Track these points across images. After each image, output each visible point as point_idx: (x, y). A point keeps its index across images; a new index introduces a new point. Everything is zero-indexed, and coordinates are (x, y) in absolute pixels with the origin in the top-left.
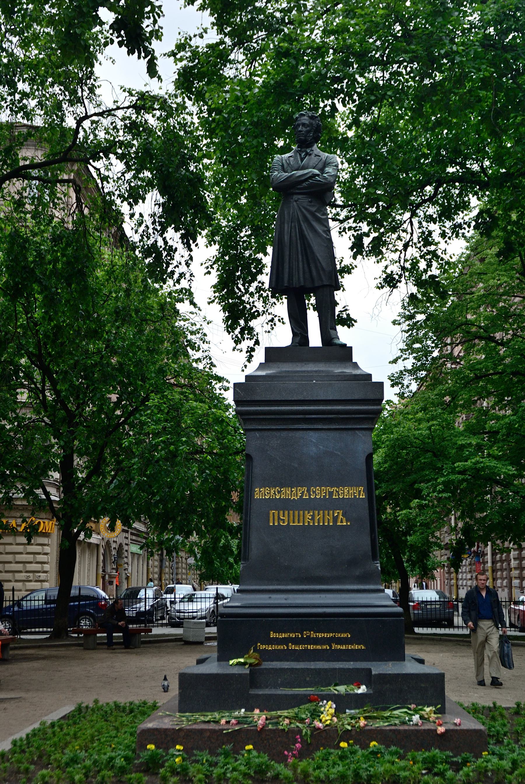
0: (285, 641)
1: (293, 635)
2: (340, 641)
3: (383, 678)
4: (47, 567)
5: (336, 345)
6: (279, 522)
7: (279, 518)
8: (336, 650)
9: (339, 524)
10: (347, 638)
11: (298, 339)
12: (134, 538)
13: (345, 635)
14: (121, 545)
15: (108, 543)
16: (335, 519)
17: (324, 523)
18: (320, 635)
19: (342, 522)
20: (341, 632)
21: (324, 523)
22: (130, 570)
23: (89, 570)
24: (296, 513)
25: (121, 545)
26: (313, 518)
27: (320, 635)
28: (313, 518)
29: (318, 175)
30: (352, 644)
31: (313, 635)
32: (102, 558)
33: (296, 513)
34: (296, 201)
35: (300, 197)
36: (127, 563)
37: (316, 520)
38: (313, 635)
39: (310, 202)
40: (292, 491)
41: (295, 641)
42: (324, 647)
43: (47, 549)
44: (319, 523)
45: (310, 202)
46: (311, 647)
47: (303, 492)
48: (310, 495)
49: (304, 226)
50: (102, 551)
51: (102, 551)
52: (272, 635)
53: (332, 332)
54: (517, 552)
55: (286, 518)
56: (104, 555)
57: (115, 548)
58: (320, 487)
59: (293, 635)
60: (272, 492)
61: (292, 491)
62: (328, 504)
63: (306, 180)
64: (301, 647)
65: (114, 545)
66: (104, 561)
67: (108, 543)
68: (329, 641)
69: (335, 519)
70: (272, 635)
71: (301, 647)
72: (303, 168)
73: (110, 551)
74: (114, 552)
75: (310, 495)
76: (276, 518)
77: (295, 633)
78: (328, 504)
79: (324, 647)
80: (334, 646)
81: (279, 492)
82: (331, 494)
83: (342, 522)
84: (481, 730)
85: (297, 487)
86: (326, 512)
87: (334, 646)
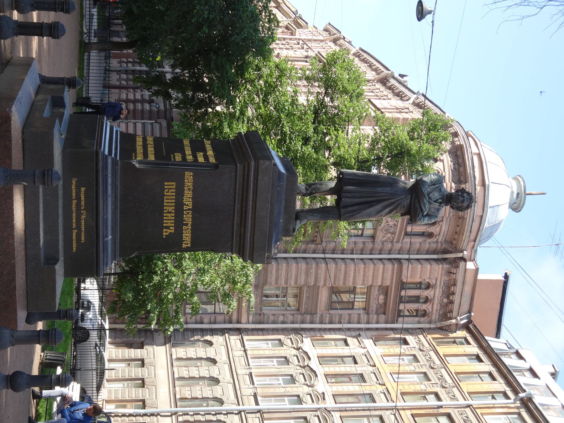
0: (78, 198)
9: (164, 230)
10: (81, 240)
16: (168, 228)
18: (83, 222)
19: (166, 232)
26: (169, 212)
27: (83, 222)
31: (83, 217)
33: (174, 201)
35: (409, 201)
38: (83, 217)
40: (189, 198)
41: (78, 205)
42: (74, 225)
44: (166, 216)
52: (83, 189)
60: (189, 184)
61: (189, 198)
63: (420, 206)
69: (168, 228)
70: (83, 189)
75: (186, 210)
77: (85, 205)
78: (179, 223)
79: (74, 225)
80: (75, 232)
82: (187, 225)
83: (166, 232)
87: (75, 232)
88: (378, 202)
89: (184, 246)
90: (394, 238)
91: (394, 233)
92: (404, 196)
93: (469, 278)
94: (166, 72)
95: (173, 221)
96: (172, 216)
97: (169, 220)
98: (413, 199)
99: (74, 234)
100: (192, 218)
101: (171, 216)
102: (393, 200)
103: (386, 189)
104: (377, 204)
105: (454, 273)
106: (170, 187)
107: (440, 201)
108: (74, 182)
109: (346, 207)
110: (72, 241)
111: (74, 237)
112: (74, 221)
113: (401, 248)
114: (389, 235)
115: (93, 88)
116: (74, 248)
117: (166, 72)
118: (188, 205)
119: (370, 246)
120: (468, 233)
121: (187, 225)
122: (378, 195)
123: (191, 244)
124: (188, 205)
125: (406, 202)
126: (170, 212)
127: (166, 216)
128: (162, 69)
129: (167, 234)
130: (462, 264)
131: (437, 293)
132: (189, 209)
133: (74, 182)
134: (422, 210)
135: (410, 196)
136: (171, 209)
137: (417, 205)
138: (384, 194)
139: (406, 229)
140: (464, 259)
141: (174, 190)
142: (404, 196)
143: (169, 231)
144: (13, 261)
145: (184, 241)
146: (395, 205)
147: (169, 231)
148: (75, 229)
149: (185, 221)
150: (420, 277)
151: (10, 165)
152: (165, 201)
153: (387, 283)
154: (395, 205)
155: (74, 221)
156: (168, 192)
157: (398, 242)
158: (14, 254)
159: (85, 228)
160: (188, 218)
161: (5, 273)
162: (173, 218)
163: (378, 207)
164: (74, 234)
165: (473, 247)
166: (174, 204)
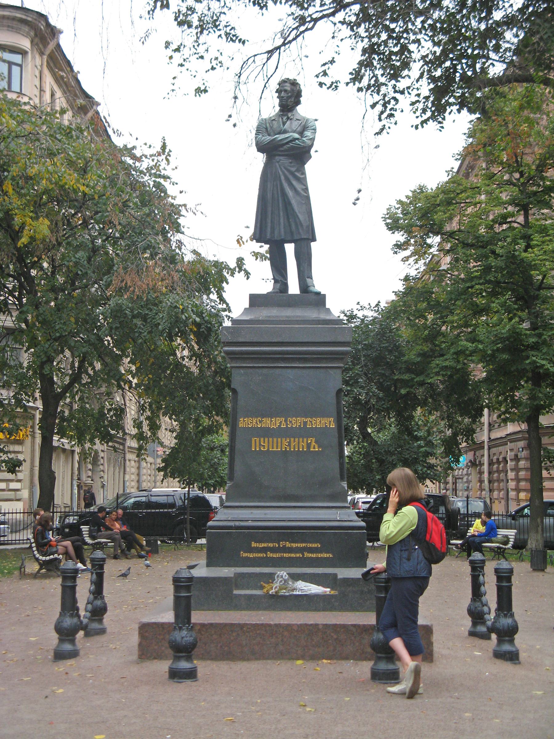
1: (270, 545)
2: (311, 550)
5: (311, 292)
7: (260, 444)
10: (316, 548)
11: (278, 285)
16: (309, 445)
17: (299, 448)
18: (294, 545)
19: (314, 448)
21: (299, 448)
26: (289, 445)
27: (294, 545)
29: (298, 139)
31: (288, 545)
32: (76, 465)
33: (275, 440)
34: (278, 162)
35: (282, 158)
38: (288, 545)
40: (271, 421)
41: (273, 550)
42: (298, 555)
44: (294, 448)
46: (286, 555)
48: (287, 424)
50: (77, 457)
51: (77, 457)
52: (254, 545)
54: (514, 463)
59: (270, 545)
60: (254, 421)
61: (271, 421)
64: (278, 555)
66: (79, 469)
69: (309, 445)
70: (254, 545)
71: (278, 555)
75: (287, 424)
79: (298, 555)
80: (306, 555)
81: (260, 422)
82: (305, 423)
87: (306, 555)
92: (277, 164)
94: (490, 438)
96: (294, 441)
97: (299, 445)
99: (310, 555)
100: (296, 417)
102: (283, 178)
103: (269, 186)
104: (287, 196)
106: (259, 444)
107: (285, 118)
108: (245, 555)
109: (292, 233)
110: (318, 558)
111: (314, 556)
112: (293, 555)
116: (262, 555)
117: (490, 438)
118: (281, 423)
122: (276, 196)
124: (281, 423)
125: (285, 161)
126: (289, 443)
127: (294, 448)
128: (486, 443)
129: (316, 447)
132: (286, 421)
133: (245, 555)
135: (277, 158)
136: (285, 443)
138: (275, 188)
141: (262, 439)
142: (277, 164)
144: (321, 627)
145: (326, 426)
148: (303, 555)
149: (300, 426)
151: (169, 624)
155: (293, 555)
158: (312, 625)
161: (335, 637)
162: (297, 439)
163: (290, 193)
164: (310, 555)
166: (279, 440)
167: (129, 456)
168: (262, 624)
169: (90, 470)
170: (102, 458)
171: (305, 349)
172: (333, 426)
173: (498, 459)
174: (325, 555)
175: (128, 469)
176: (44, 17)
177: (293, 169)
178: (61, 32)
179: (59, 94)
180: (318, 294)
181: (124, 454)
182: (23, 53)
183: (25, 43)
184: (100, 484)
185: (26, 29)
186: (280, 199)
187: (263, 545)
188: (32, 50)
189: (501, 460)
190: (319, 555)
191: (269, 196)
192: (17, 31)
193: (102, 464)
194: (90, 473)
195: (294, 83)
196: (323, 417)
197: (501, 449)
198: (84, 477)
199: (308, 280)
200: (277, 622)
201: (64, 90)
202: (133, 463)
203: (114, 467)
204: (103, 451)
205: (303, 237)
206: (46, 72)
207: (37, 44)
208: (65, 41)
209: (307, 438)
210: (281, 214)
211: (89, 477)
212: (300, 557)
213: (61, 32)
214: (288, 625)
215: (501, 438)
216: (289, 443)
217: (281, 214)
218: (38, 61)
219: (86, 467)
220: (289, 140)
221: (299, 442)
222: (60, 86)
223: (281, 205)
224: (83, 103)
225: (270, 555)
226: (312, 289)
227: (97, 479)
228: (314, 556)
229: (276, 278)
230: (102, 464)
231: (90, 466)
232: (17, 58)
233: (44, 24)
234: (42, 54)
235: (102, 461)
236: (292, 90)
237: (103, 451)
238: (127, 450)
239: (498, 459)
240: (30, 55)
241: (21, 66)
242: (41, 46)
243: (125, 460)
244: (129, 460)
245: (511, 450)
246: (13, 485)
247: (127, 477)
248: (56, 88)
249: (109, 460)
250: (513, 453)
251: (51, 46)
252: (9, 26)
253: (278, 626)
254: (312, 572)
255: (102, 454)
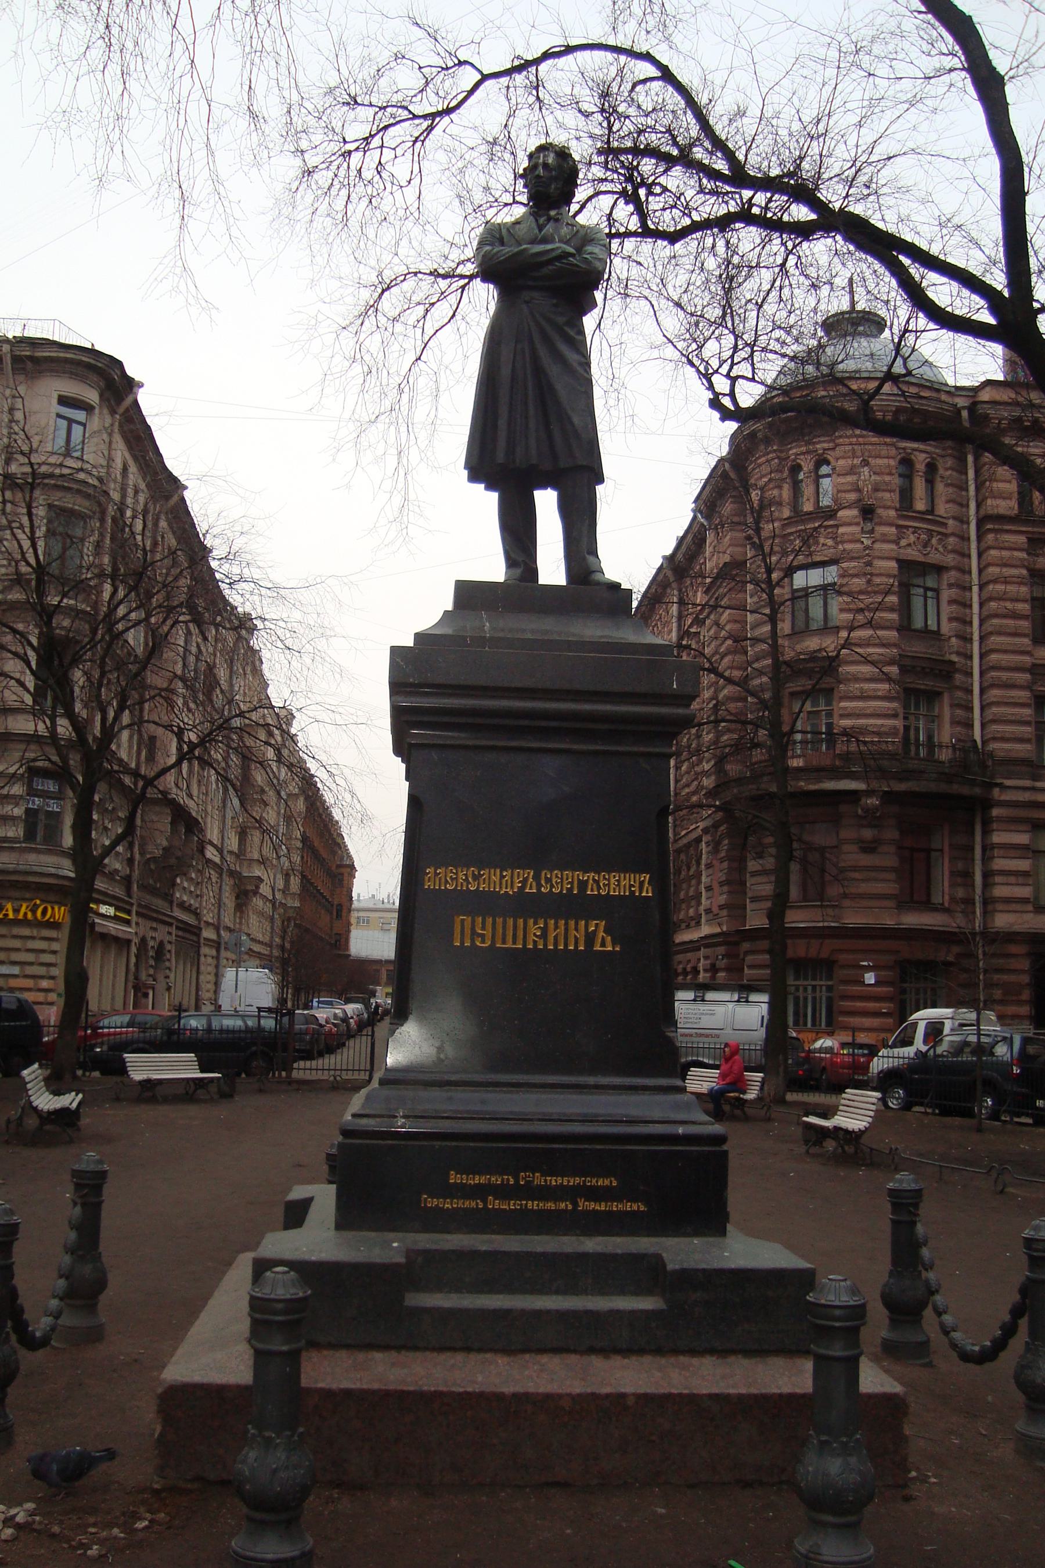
0: (480, 1192)
1: (496, 1180)
2: (594, 1194)
3: (688, 1278)
4: (55, 971)
5: (598, 583)
6: (473, 941)
7: (473, 932)
8: (587, 1213)
9: (597, 948)
10: (608, 1189)
11: (518, 572)
12: (180, 933)
13: (607, 1182)
14: (161, 943)
15: (143, 941)
16: (590, 938)
17: (566, 945)
18: (553, 1181)
19: (603, 944)
20: (599, 1176)
21: (566, 945)
22: (172, 976)
23: (115, 976)
24: (510, 922)
25: (161, 943)
26: (544, 935)
27: (553, 1181)
28: (544, 935)
29: (572, 255)
30: (619, 1200)
31: (538, 1179)
32: (133, 960)
33: (510, 922)
34: (527, 302)
35: (535, 294)
36: (170, 969)
37: (572, 940)
38: (538, 1179)
39: (556, 306)
40: (502, 877)
41: (503, 1192)
42: (563, 1206)
43: (55, 946)
44: (556, 944)
45: (556, 306)
46: (533, 1205)
47: (526, 880)
48: (539, 886)
49: (543, 352)
50: (134, 950)
51: (134, 950)
52: (454, 1178)
53: (591, 559)
54: (708, 975)
55: (488, 933)
56: (137, 956)
57: (153, 947)
58: (562, 871)
59: (496, 1180)
60: (461, 876)
61: (502, 877)
62: (574, 906)
63: (550, 262)
64: (513, 1205)
65: (151, 943)
66: (137, 965)
67: (143, 941)
68: (572, 1194)
69: (590, 938)
70: (454, 1178)
71: (513, 1205)
72: (545, 240)
73: (146, 950)
74: (151, 953)
75: (539, 886)
76: (468, 931)
77: (502, 1174)
78: (574, 906)
79: (563, 1206)
80: (583, 1205)
81: (476, 878)
82: (583, 885)
83: (603, 944)
84: (896, 1395)
85: (513, 869)
86: (572, 923)
87: (583, 1205)
88: (539, 371)
89: (648, 892)
90: (939, 533)
91: (930, 533)
93: (1006, 395)
95: (572, 923)
96: (556, 927)
97: (568, 935)
98: (530, 283)
99: (592, 1206)
101: (556, 929)
105: (1000, 422)
108: (433, 1203)
110: (610, 1213)
111: (602, 1207)
112: (550, 1205)
113: (955, 518)
114: (934, 541)
115: (1014, 964)
116: (473, 1204)
118: (525, 881)
119: (952, 576)
120: (924, 402)
121: (583, 885)
123: (641, 872)
124: (525, 881)
126: (545, 931)
130: (980, 410)
131: (1037, 451)
132: (537, 878)
133: (433, 1203)
134: (559, 258)
137: (545, 271)
139: (919, 512)
140: (972, 408)
143: (601, 934)
146: (548, 328)
147: (601, 934)
148: (575, 1204)
149: (570, 890)
150: (1010, 482)
152: (509, 945)
153: (1022, 539)
154: (548, 328)
155: (550, 1205)
156: (483, 936)
157: (945, 525)
159: (574, 1175)
160: (561, 881)
163: (553, 370)
164: (592, 1206)
165: (948, 393)
167: (205, 950)
168: (481, 1394)
169: (151, 966)
170: (169, 951)
171: (587, 707)
172: (648, 892)
173: (685, 969)
174: (629, 1206)
175: (202, 968)
176: (119, 364)
177: (561, 320)
178: (140, 385)
179: (133, 468)
180: (615, 586)
181: (199, 947)
182: (88, 408)
183: (92, 396)
184: (165, 986)
185: (95, 378)
186: (530, 384)
187: (478, 1180)
188: (101, 407)
189: (689, 969)
190: (615, 1207)
191: (506, 372)
192: (83, 379)
193: (169, 960)
194: (151, 971)
195: (563, 154)
196: (625, 871)
197: (689, 955)
198: (143, 977)
199: (591, 559)
200: (519, 1389)
201: (140, 464)
202: (209, 960)
203: (184, 963)
204: (170, 942)
205: (580, 463)
206: (118, 438)
207: (108, 400)
208: (145, 399)
209: (588, 918)
210: (532, 411)
211: (150, 976)
212: (566, 1211)
213: (140, 385)
214: (548, 1396)
215: (691, 942)
216: (545, 931)
217: (532, 411)
218: (108, 420)
219: (147, 962)
220: (554, 254)
221: (566, 930)
222: (135, 458)
223: (530, 393)
224: (166, 488)
225: (494, 1203)
226: (597, 577)
227: (160, 977)
228: (602, 1207)
229: (513, 555)
230: (169, 960)
231: (152, 962)
232: (80, 415)
233: (119, 373)
234: (113, 412)
235: (168, 956)
236: (560, 167)
237: (170, 942)
238: (202, 941)
239: (685, 969)
240: (97, 411)
241: (84, 425)
242: (112, 402)
243: (199, 955)
244: (205, 956)
245: (706, 958)
246: (45, 984)
247: (202, 977)
248: (131, 462)
249: (177, 954)
250: (708, 962)
251: (129, 400)
252: (71, 373)
253: (522, 1398)
254: (599, 1249)
255: (168, 947)
